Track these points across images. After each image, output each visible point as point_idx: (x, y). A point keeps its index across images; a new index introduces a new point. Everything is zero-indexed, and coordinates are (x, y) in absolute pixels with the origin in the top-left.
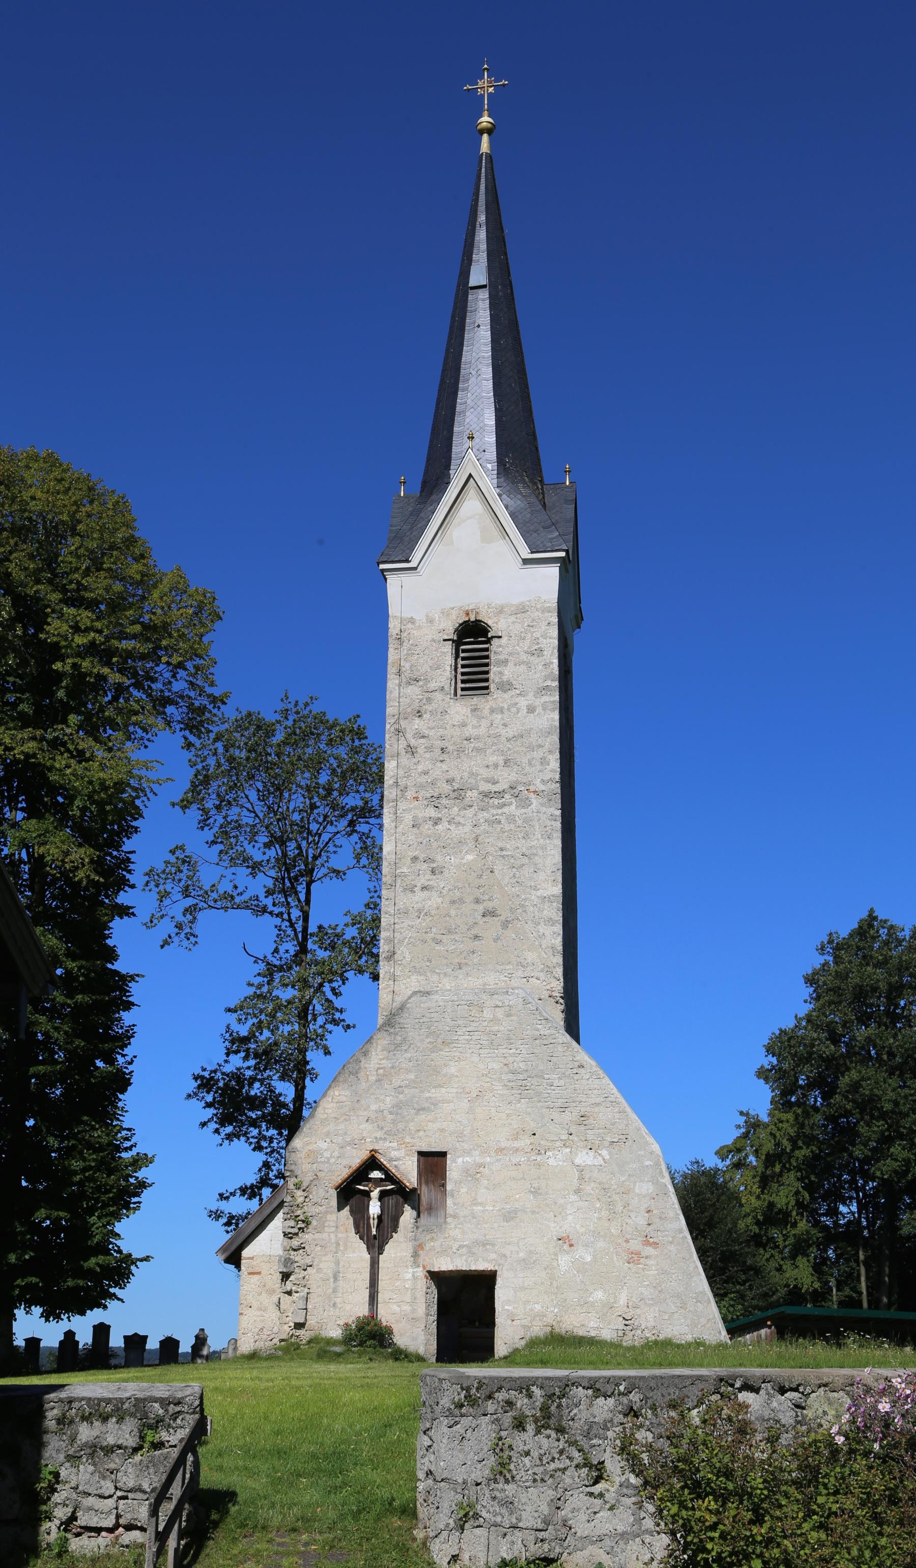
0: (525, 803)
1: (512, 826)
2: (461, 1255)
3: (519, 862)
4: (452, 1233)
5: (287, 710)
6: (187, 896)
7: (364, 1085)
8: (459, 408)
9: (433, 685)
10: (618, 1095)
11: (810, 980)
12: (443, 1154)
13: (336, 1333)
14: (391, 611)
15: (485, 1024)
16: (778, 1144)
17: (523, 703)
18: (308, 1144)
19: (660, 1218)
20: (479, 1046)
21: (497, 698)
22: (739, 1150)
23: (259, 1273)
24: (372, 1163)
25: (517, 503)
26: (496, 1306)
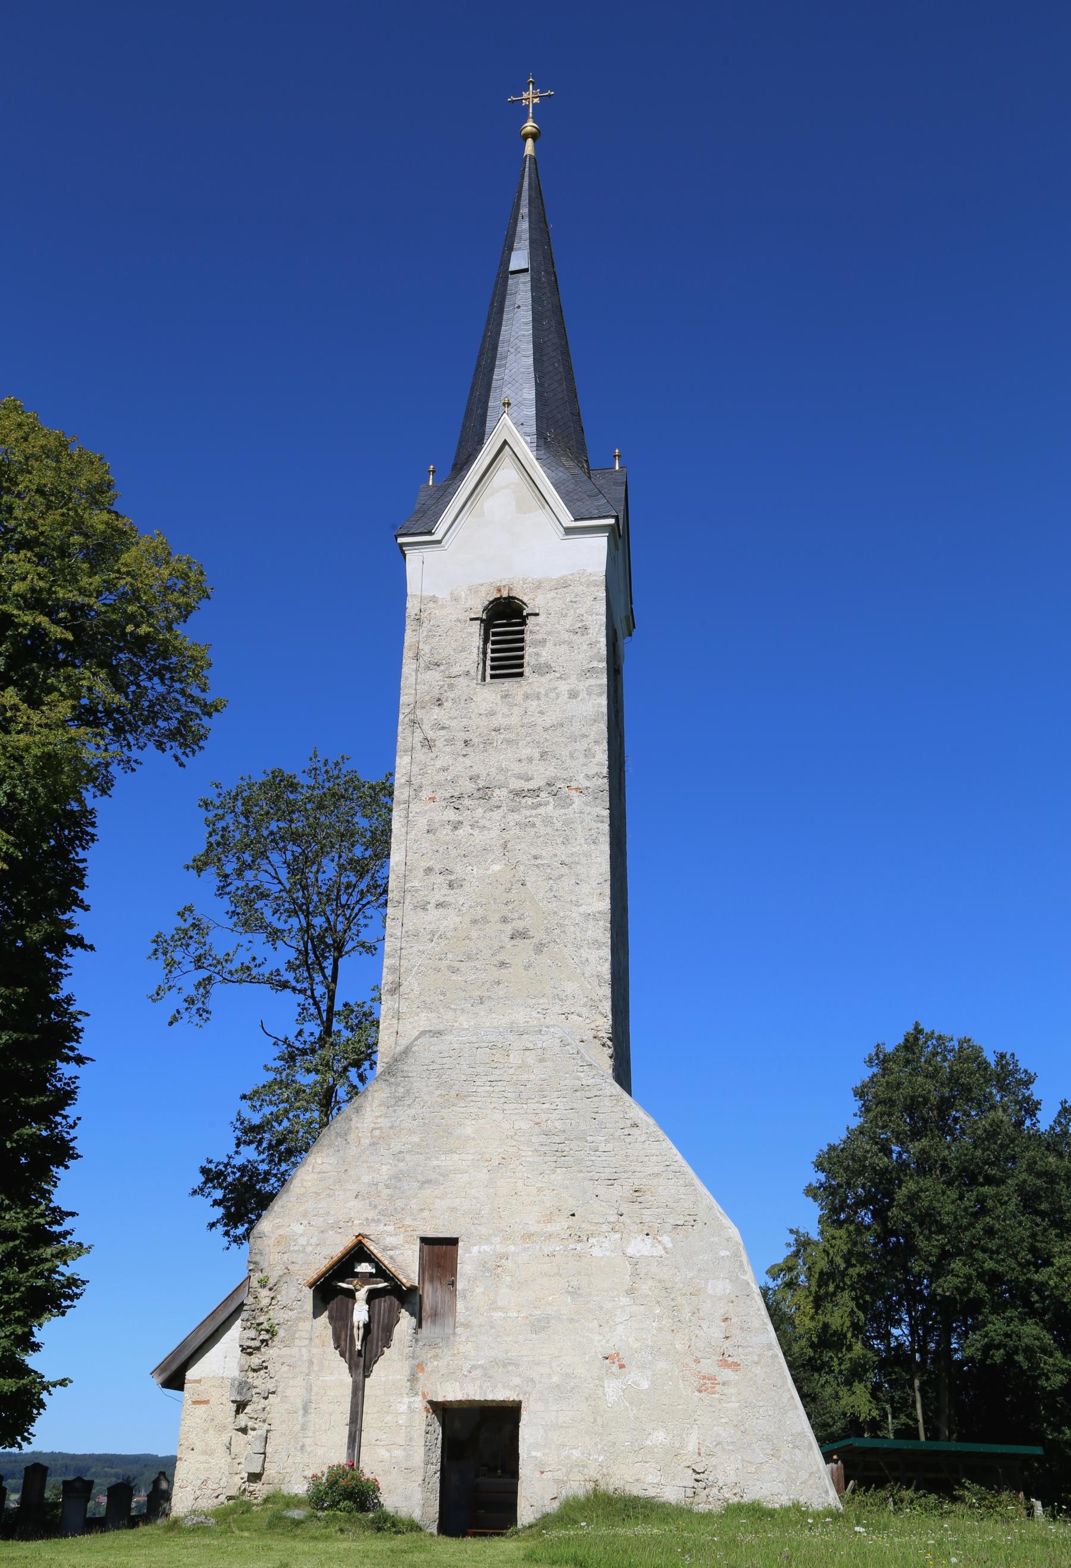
0: (565, 803)
1: (549, 830)
2: (474, 1379)
3: (556, 873)
4: (462, 1348)
5: (315, 769)
6: (200, 967)
7: (353, 1150)
8: (494, 384)
9: (455, 670)
10: (684, 1163)
11: (860, 1093)
12: (453, 1242)
13: (300, 1488)
14: (410, 590)
15: (511, 1071)
16: (831, 1262)
17: (564, 687)
18: (279, 1227)
19: (742, 1328)
20: (503, 1100)
21: (532, 681)
22: (790, 1269)
23: (207, 1402)
24: (359, 1252)
25: (561, 474)
26: (520, 1451)
